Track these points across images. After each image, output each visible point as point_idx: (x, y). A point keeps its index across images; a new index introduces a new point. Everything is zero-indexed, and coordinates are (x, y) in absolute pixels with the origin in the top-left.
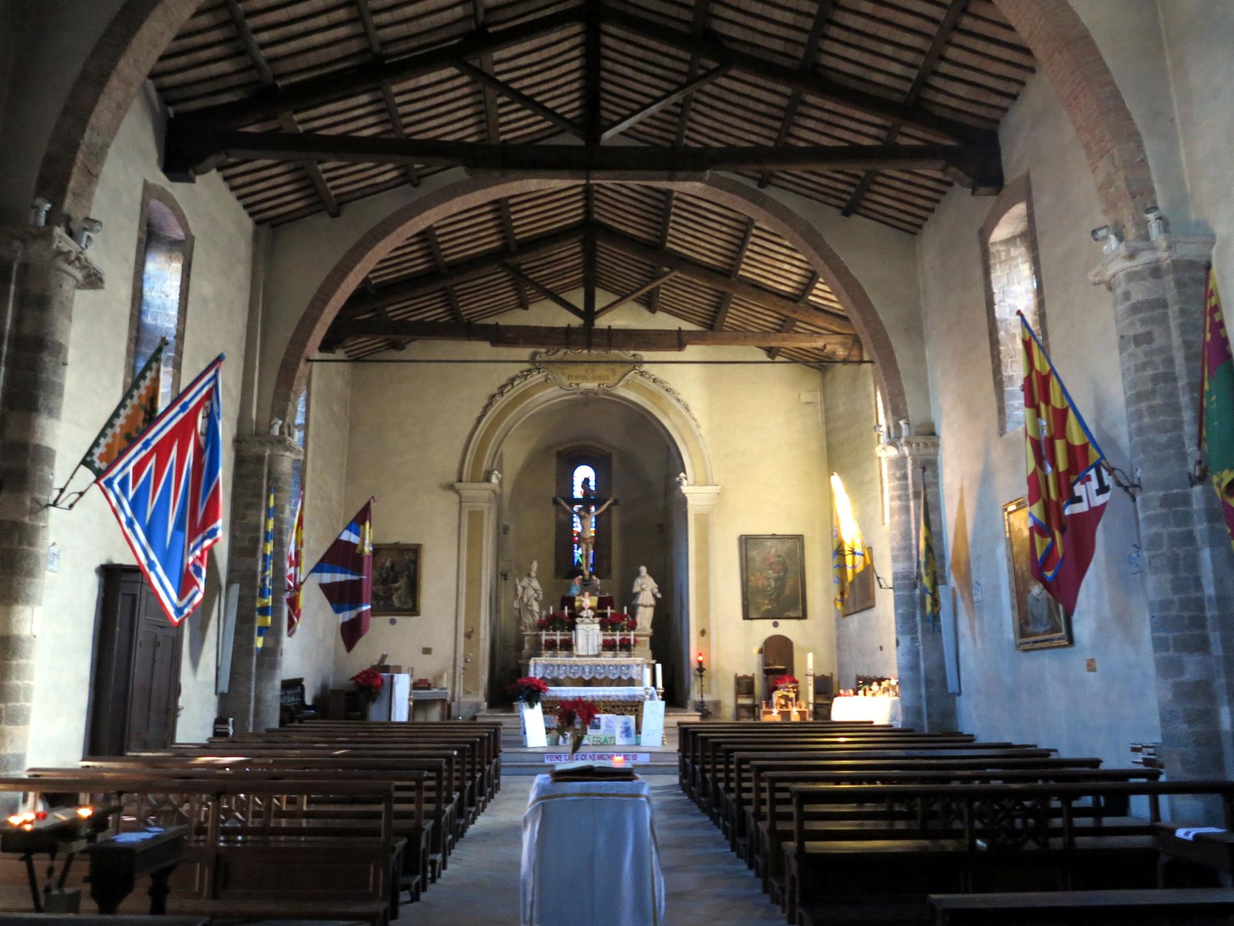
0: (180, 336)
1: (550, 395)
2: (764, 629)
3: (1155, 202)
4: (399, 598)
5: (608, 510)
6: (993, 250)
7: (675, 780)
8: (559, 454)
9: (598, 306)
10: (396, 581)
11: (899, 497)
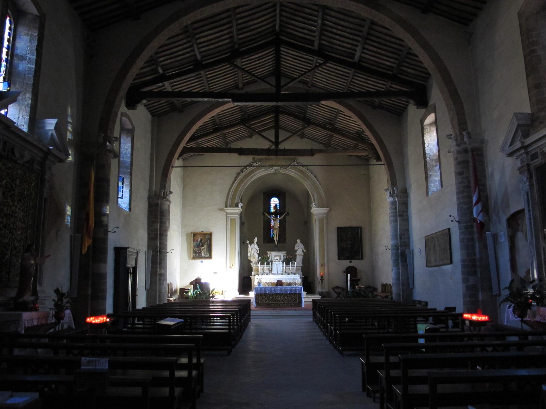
0: (131, 164)
1: (262, 173)
2: (346, 263)
3: (467, 127)
4: (204, 253)
5: (284, 218)
6: (425, 128)
7: (312, 319)
8: (264, 193)
9: (280, 140)
10: (203, 246)
11: (394, 216)
